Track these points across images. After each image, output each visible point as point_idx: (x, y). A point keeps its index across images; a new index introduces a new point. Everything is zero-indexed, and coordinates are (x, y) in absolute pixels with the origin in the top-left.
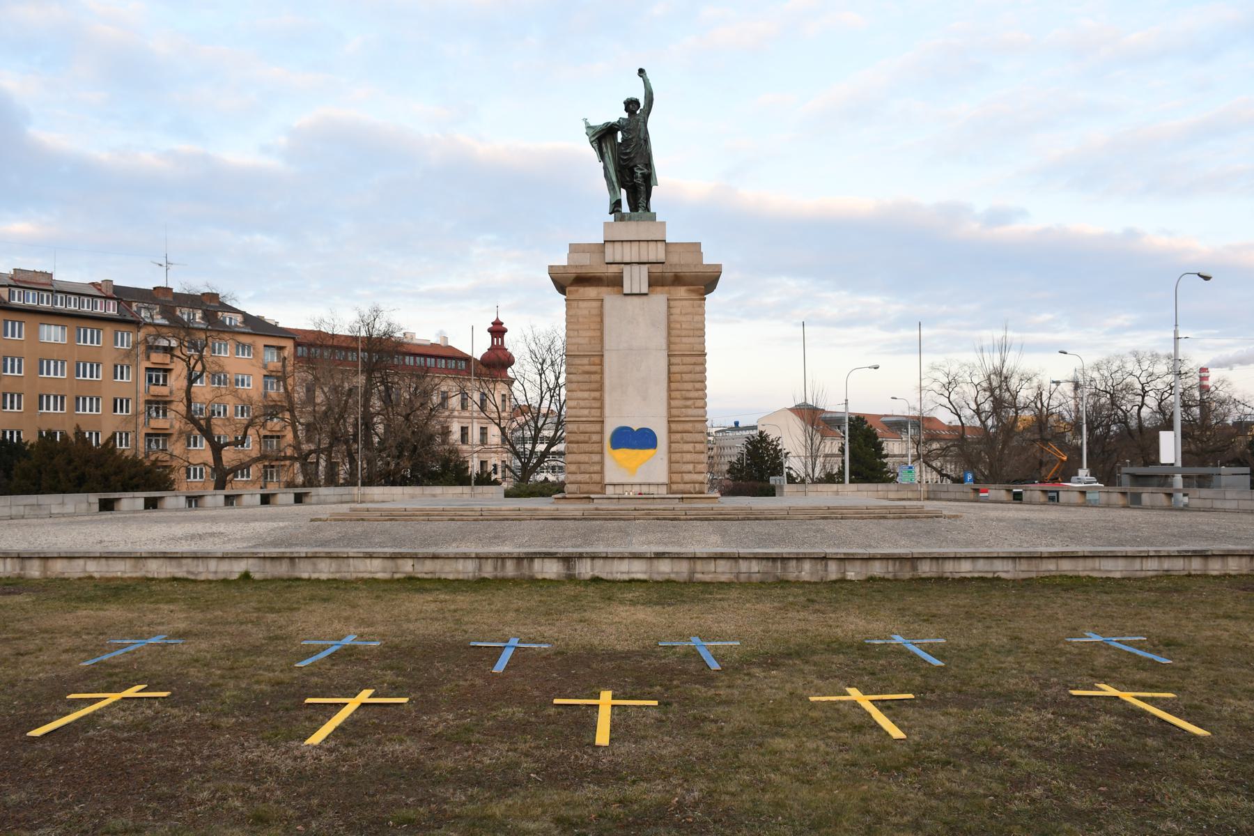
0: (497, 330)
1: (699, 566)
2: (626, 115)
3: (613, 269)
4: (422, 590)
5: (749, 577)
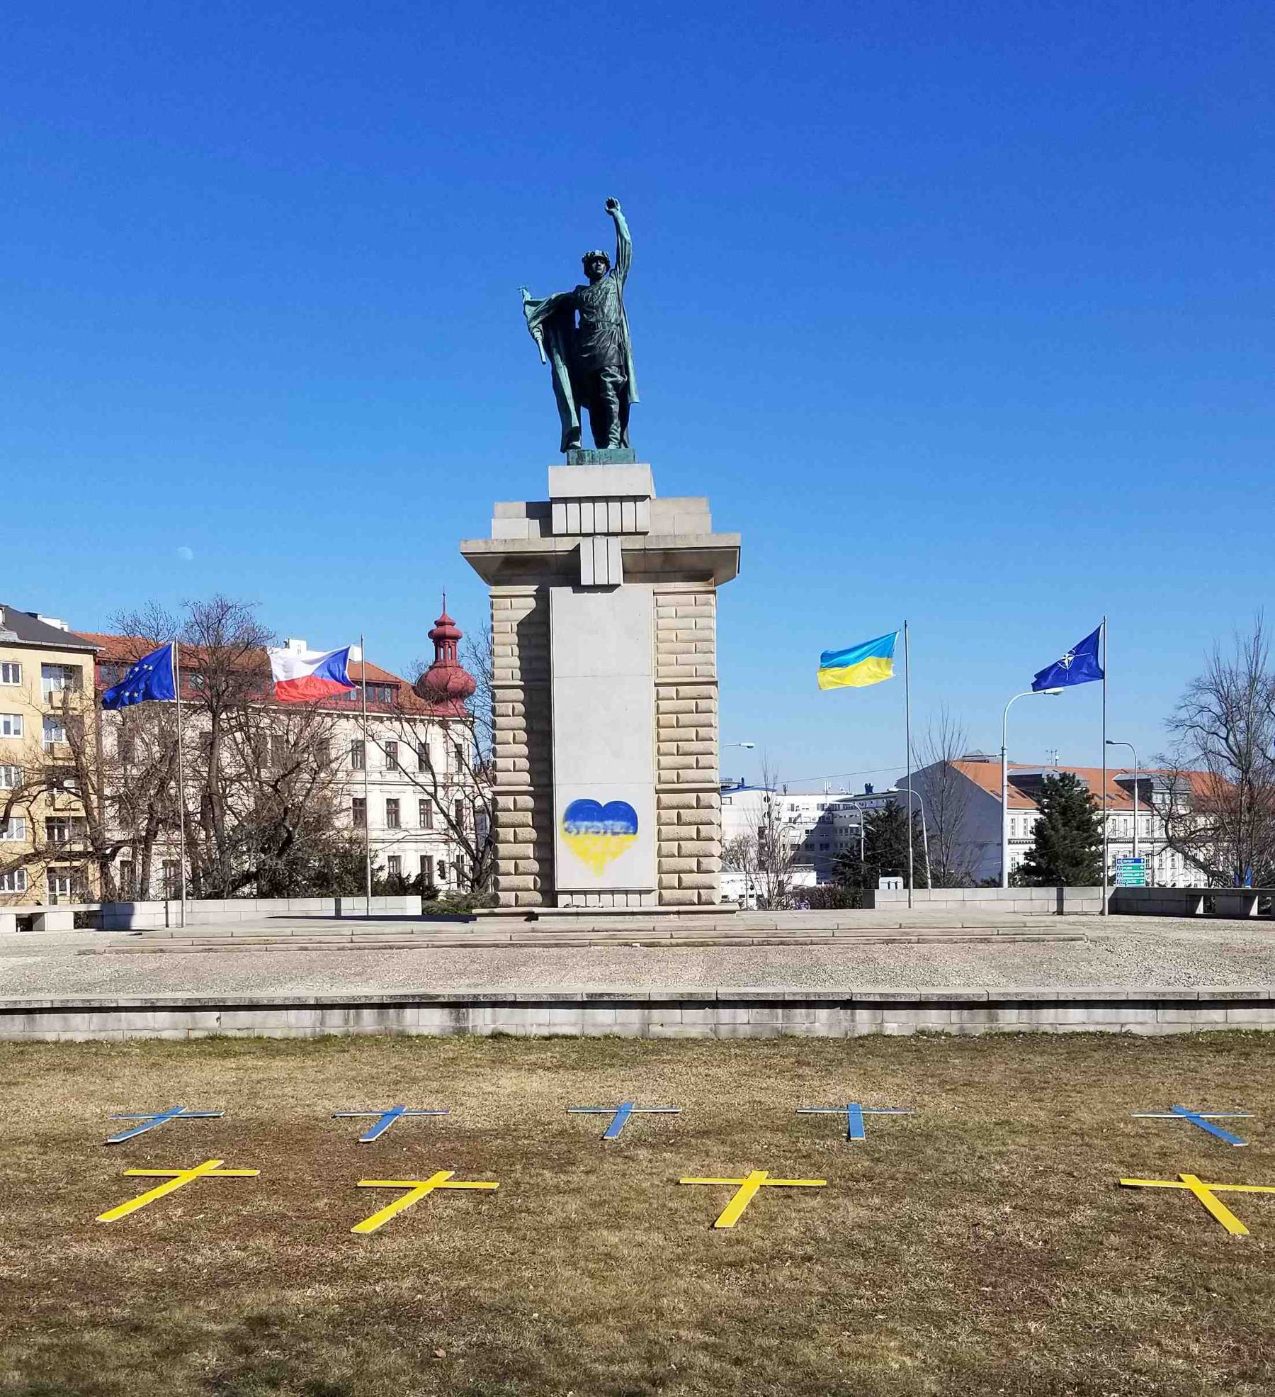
0: (442, 638)
1: (656, 1014)
2: (586, 281)
3: (566, 545)
4: (226, 1054)
5: (734, 1031)
